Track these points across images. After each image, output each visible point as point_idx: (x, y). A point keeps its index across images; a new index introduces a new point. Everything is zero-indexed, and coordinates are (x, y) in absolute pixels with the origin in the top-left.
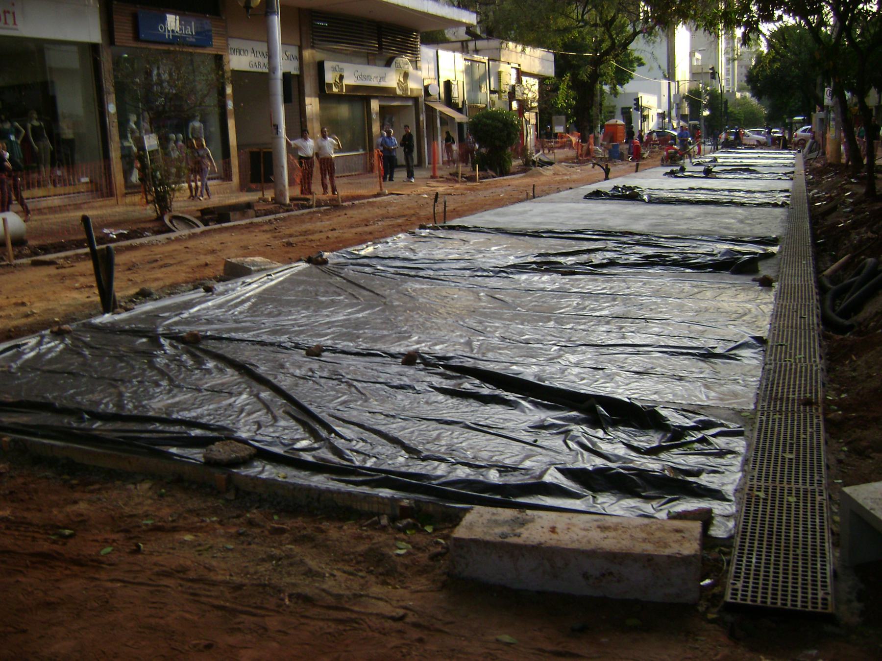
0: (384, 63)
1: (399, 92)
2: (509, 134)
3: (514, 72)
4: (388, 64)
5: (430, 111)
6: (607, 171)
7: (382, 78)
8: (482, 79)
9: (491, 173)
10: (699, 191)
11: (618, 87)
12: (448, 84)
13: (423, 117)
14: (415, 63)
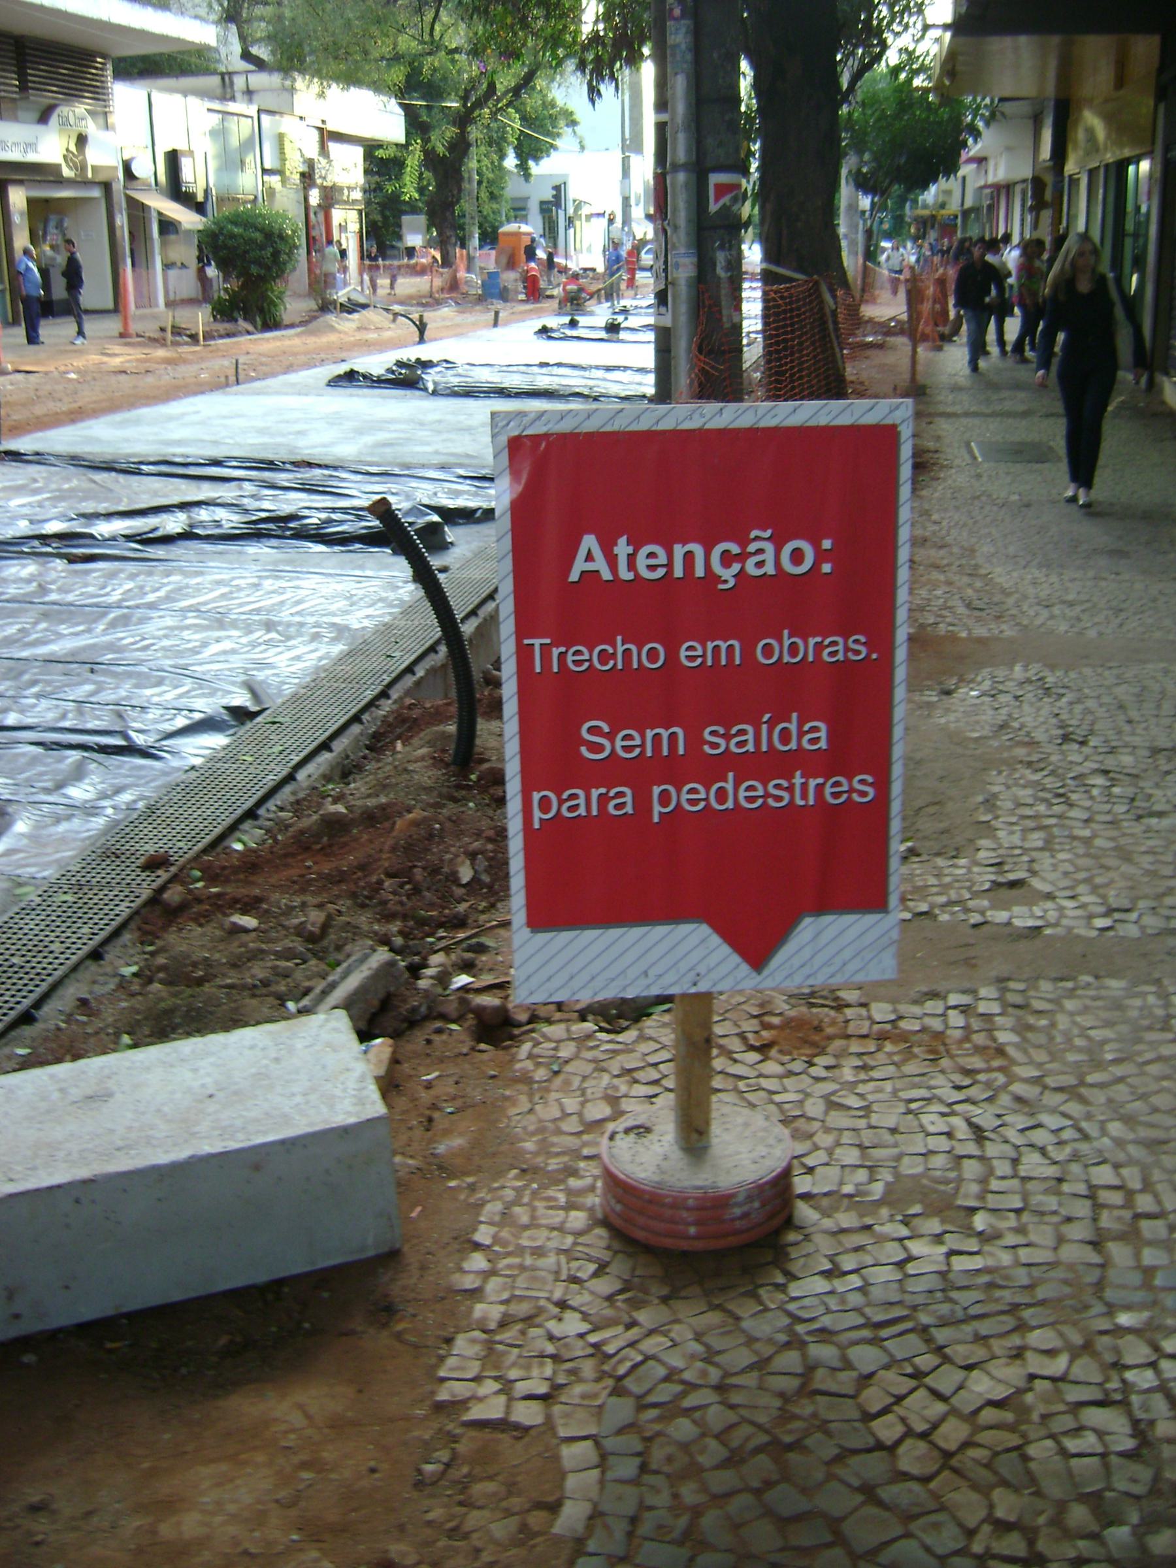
0: (36, 115)
1: (67, 172)
2: (276, 254)
3: (315, 135)
4: (44, 118)
5: (137, 210)
6: (422, 327)
7: (31, 146)
8: (247, 145)
9: (243, 324)
10: (556, 370)
11: (531, 163)
12: (173, 158)
13: (121, 220)
14: (103, 115)
